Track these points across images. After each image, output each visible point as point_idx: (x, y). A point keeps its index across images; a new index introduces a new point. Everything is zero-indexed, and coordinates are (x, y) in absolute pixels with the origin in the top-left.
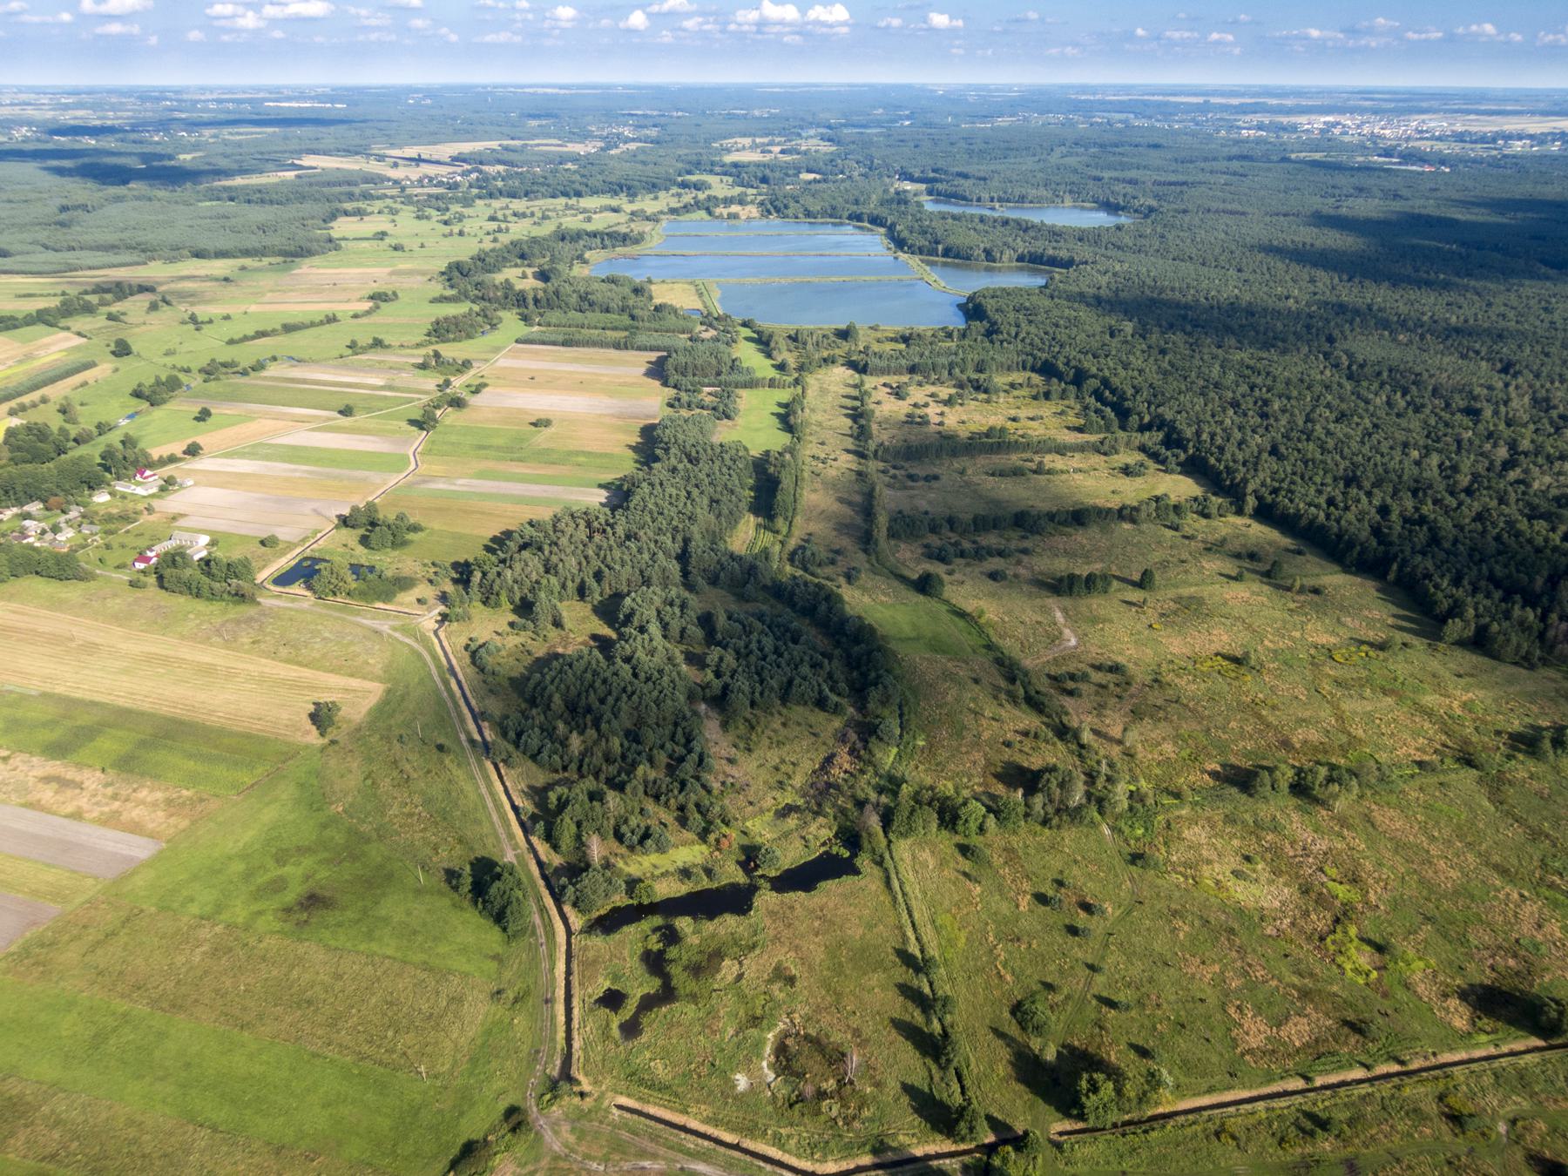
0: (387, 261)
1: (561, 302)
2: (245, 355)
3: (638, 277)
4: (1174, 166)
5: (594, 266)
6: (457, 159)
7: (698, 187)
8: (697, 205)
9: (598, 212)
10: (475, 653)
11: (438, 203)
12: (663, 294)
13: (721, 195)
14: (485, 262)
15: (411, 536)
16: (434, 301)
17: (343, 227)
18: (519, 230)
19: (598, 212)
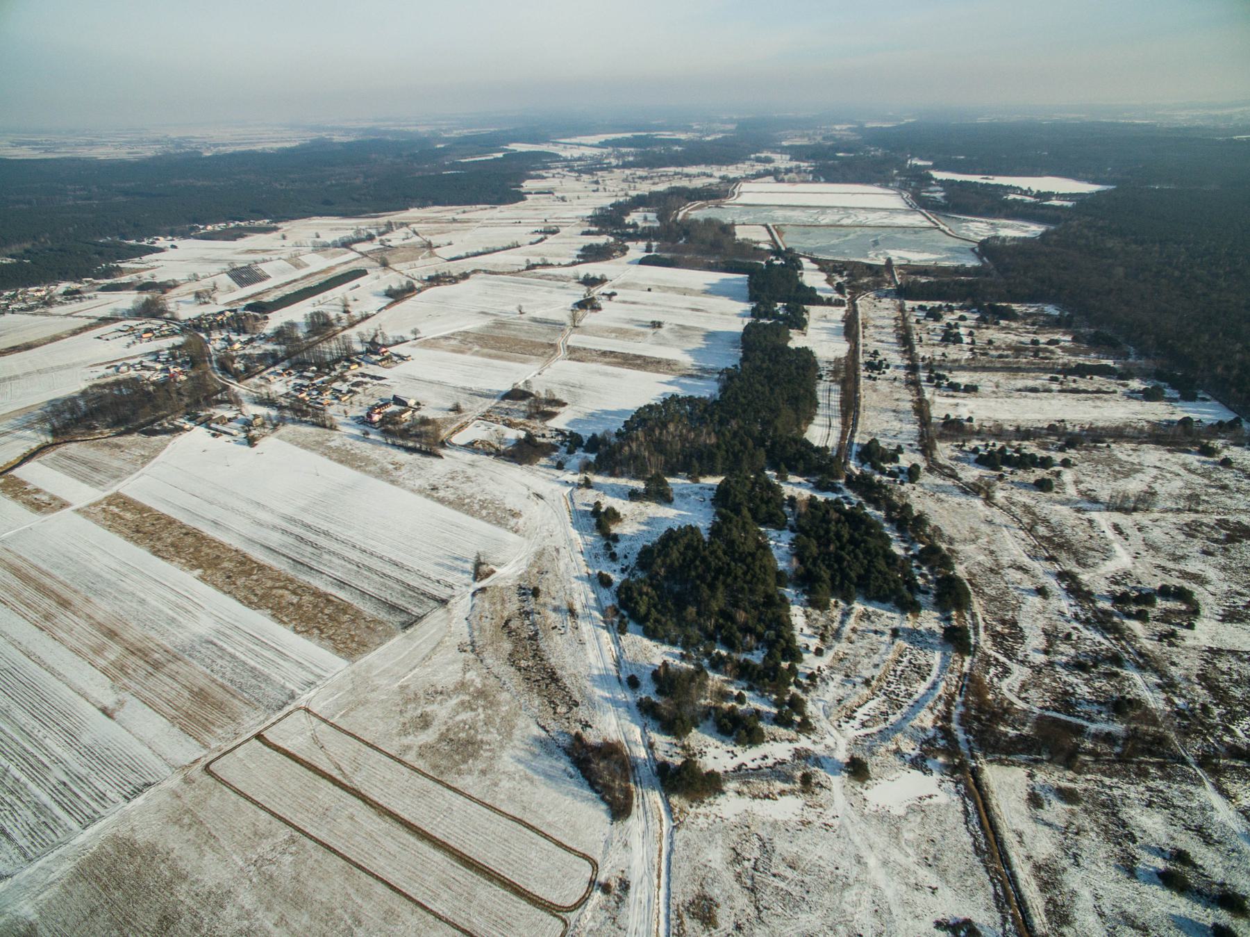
0: (572, 202)
1: (685, 241)
2: (455, 269)
3: (727, 220)
4: (156, 264)
5: (696, 212)
6: (603, 145)
7: (768, 160)
8: (767, 173)
9: (698, 176)
10: (665, 664)
11: (590, 171)
12: (741, 234)
13: (782, 166)
14: (621, 209)
15: (817, 790)
16: (584, 233)
17: (528, 185)
18: (644, 188)
19: (698, 176)
